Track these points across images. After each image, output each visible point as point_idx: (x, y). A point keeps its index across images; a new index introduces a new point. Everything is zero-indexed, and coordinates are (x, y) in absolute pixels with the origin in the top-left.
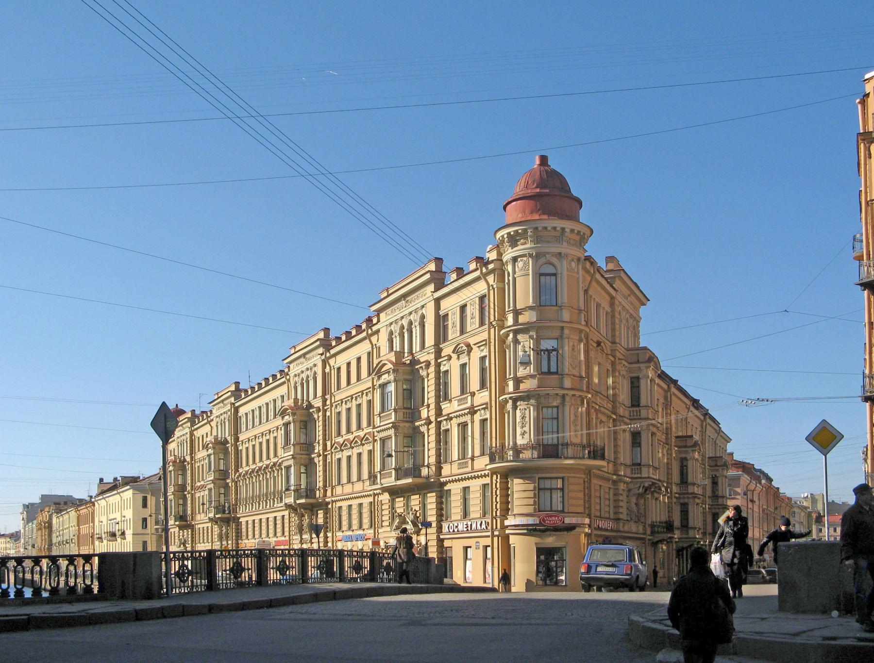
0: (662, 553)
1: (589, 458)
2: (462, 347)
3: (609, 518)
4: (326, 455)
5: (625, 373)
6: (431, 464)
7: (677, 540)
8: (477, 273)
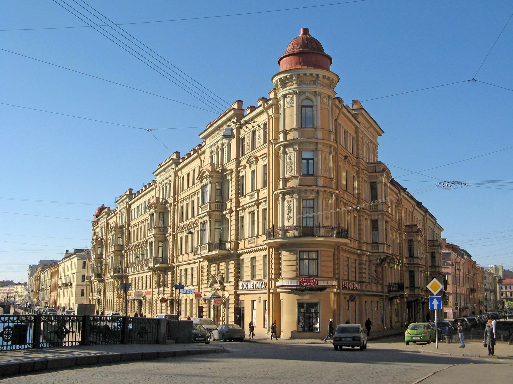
0: (397, 305)
1: (336, 237)
2: (252, 159)
3: (355, 281)
4: (174, 235)
5: (366, 179)
6: (232, 241)
7: (407, 296)
8: (261, 108)
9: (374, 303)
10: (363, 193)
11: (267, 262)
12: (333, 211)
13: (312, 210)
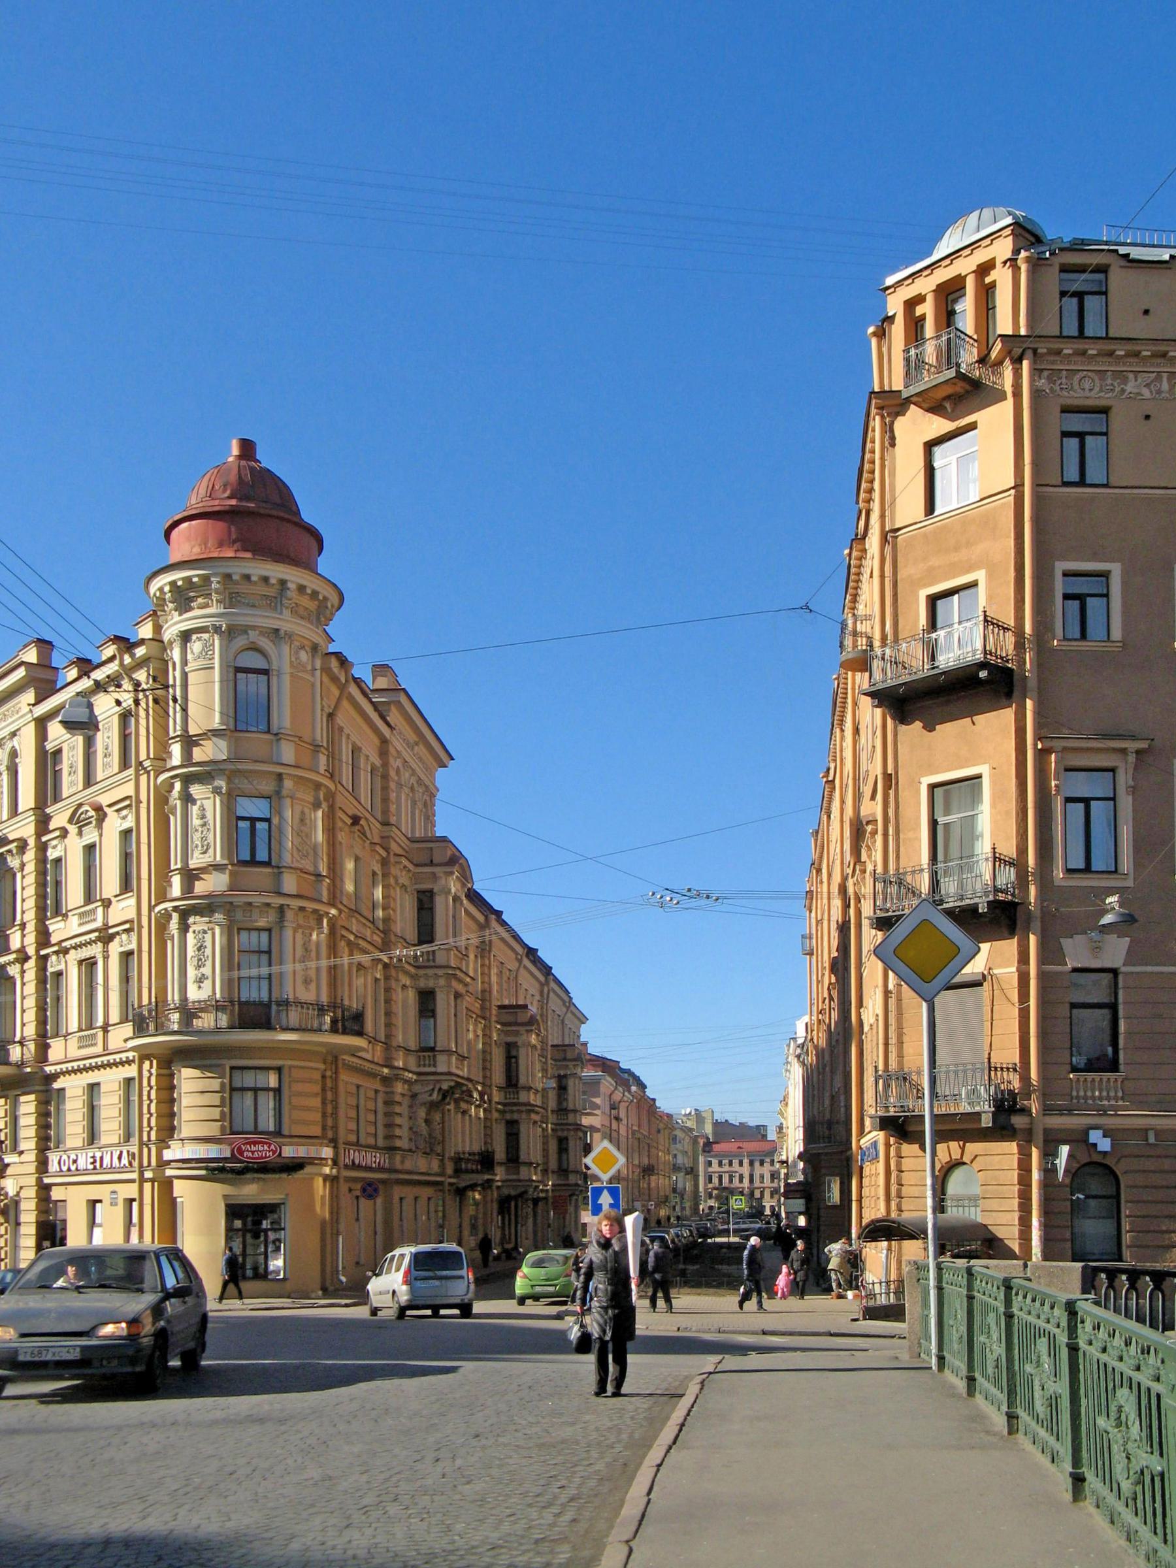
5: (407, 883)
6: (27, 1038)
7: (499, 1184)
9: (422, 1202)
10: (398, 918)
11: (135, 1098)
12: (324, 963)
13: (265, 958)
